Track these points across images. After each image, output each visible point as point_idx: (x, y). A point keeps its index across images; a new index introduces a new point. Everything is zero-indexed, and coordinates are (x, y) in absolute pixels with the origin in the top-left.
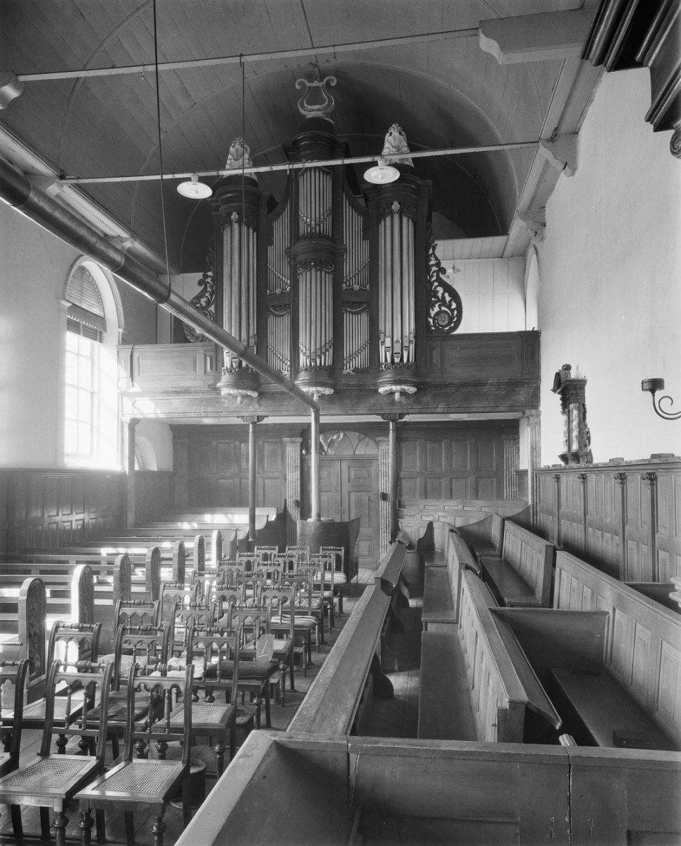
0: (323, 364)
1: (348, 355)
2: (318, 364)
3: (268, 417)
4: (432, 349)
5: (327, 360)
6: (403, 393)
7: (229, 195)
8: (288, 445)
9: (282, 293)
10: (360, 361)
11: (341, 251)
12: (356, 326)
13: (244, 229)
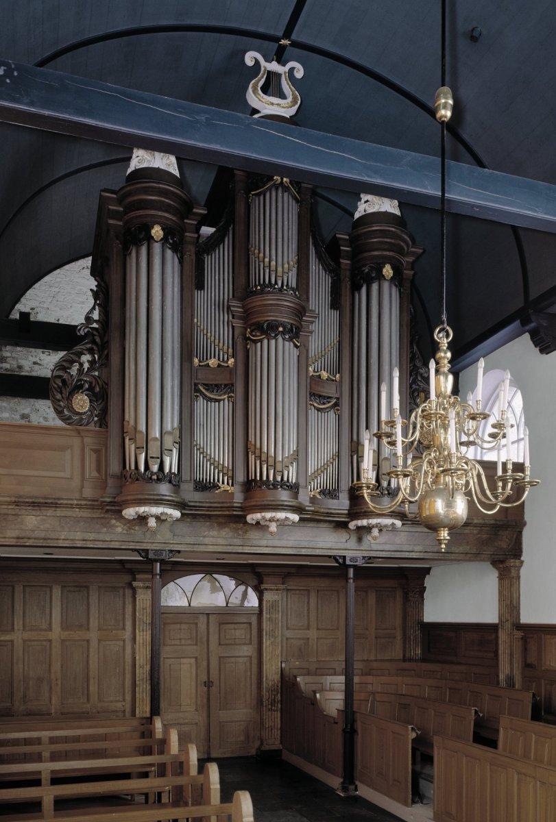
0: (265, 478)
8: (139, 591)
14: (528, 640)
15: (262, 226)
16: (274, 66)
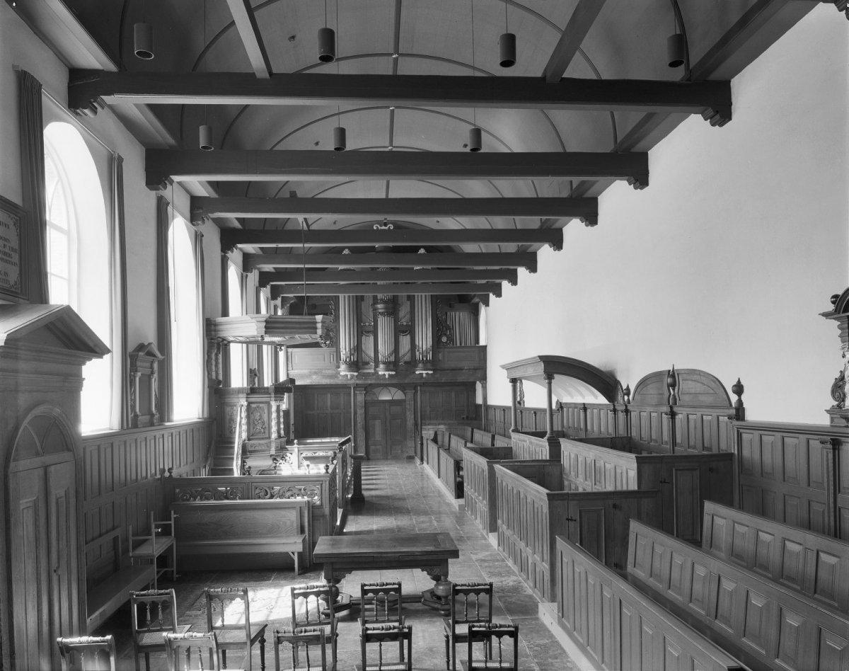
5: (392, 359)
7: (342, 283)
10: (407, 358)
11: (476, 300)
12: (405, 341)
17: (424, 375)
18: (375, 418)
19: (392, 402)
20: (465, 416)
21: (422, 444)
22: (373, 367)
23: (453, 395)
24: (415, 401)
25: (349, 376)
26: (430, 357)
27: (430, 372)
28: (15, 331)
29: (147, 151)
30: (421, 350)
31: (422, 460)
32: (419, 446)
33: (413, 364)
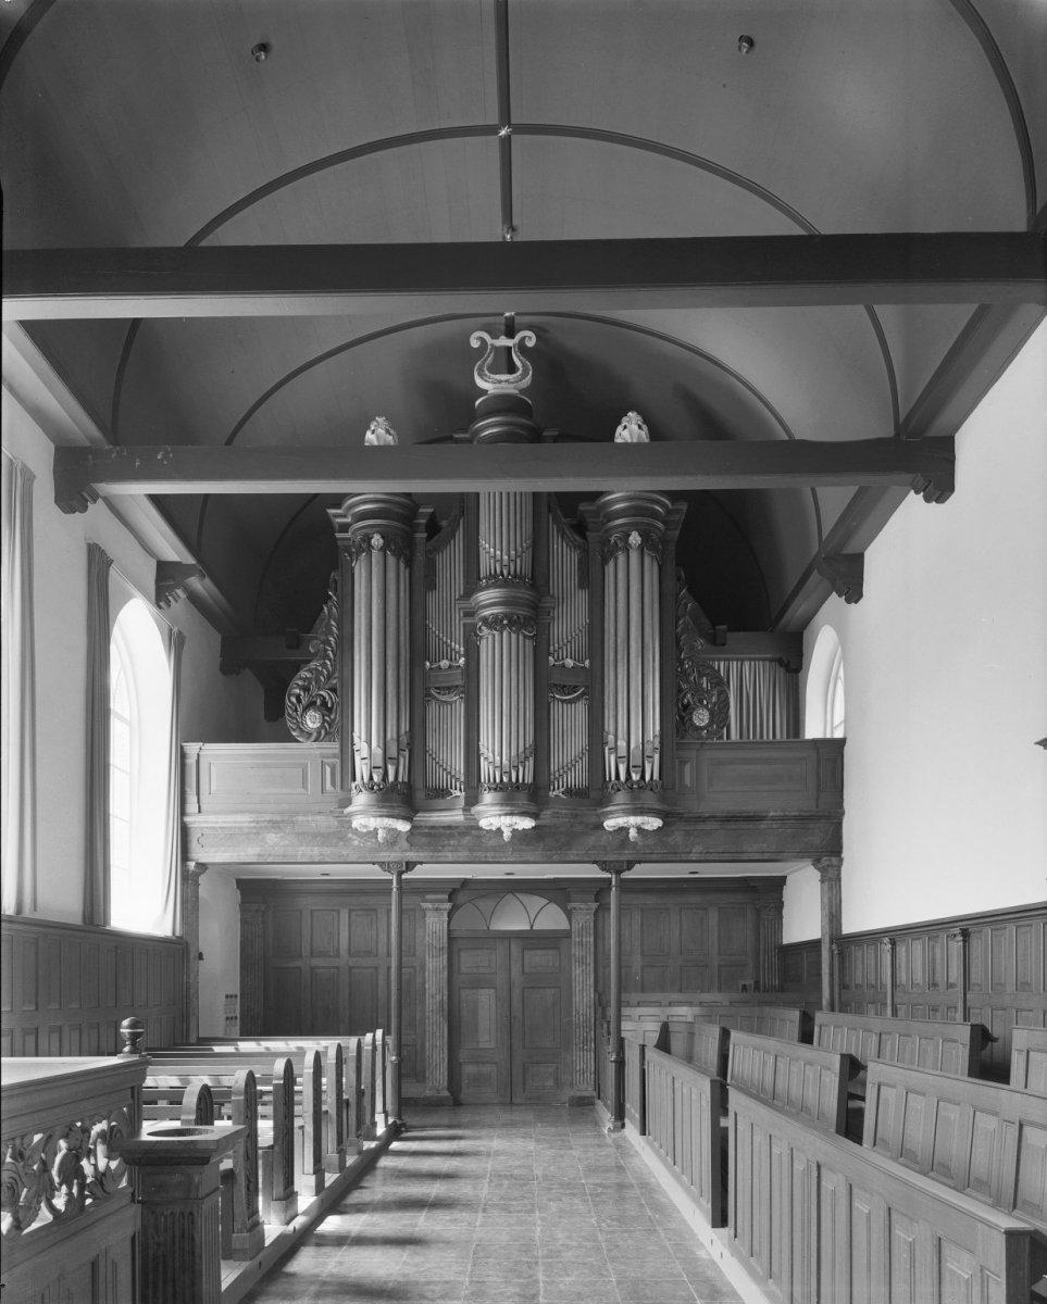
0: (521, 781)
1: (556, 769)
2: (514, 780)
3: (421, 863)
4: (683, 763)
5: (526, 774)
6: (640, 830)
8: (428, 914)
9: (450, 667)
10: (578, 777)
12: (571, 719)
13: (391, 560)
14: (533, 964)
15: (518, 510)
16: (503, 341)
17: (633, 833)
18: (477, 983)
19: (532, 940)
20: (750, 982)
21: (621, 1064)
22: (462, 802)
23: (713, 918)
24: (599, 934)
25: (381, 834)
26: (652, 769)
27: (654, 823)
28: (182, 903)
29: (57, 449)
30: (622, 744)
31: (620, 1114)
32: (611, 1069)
33: (593, 794)
